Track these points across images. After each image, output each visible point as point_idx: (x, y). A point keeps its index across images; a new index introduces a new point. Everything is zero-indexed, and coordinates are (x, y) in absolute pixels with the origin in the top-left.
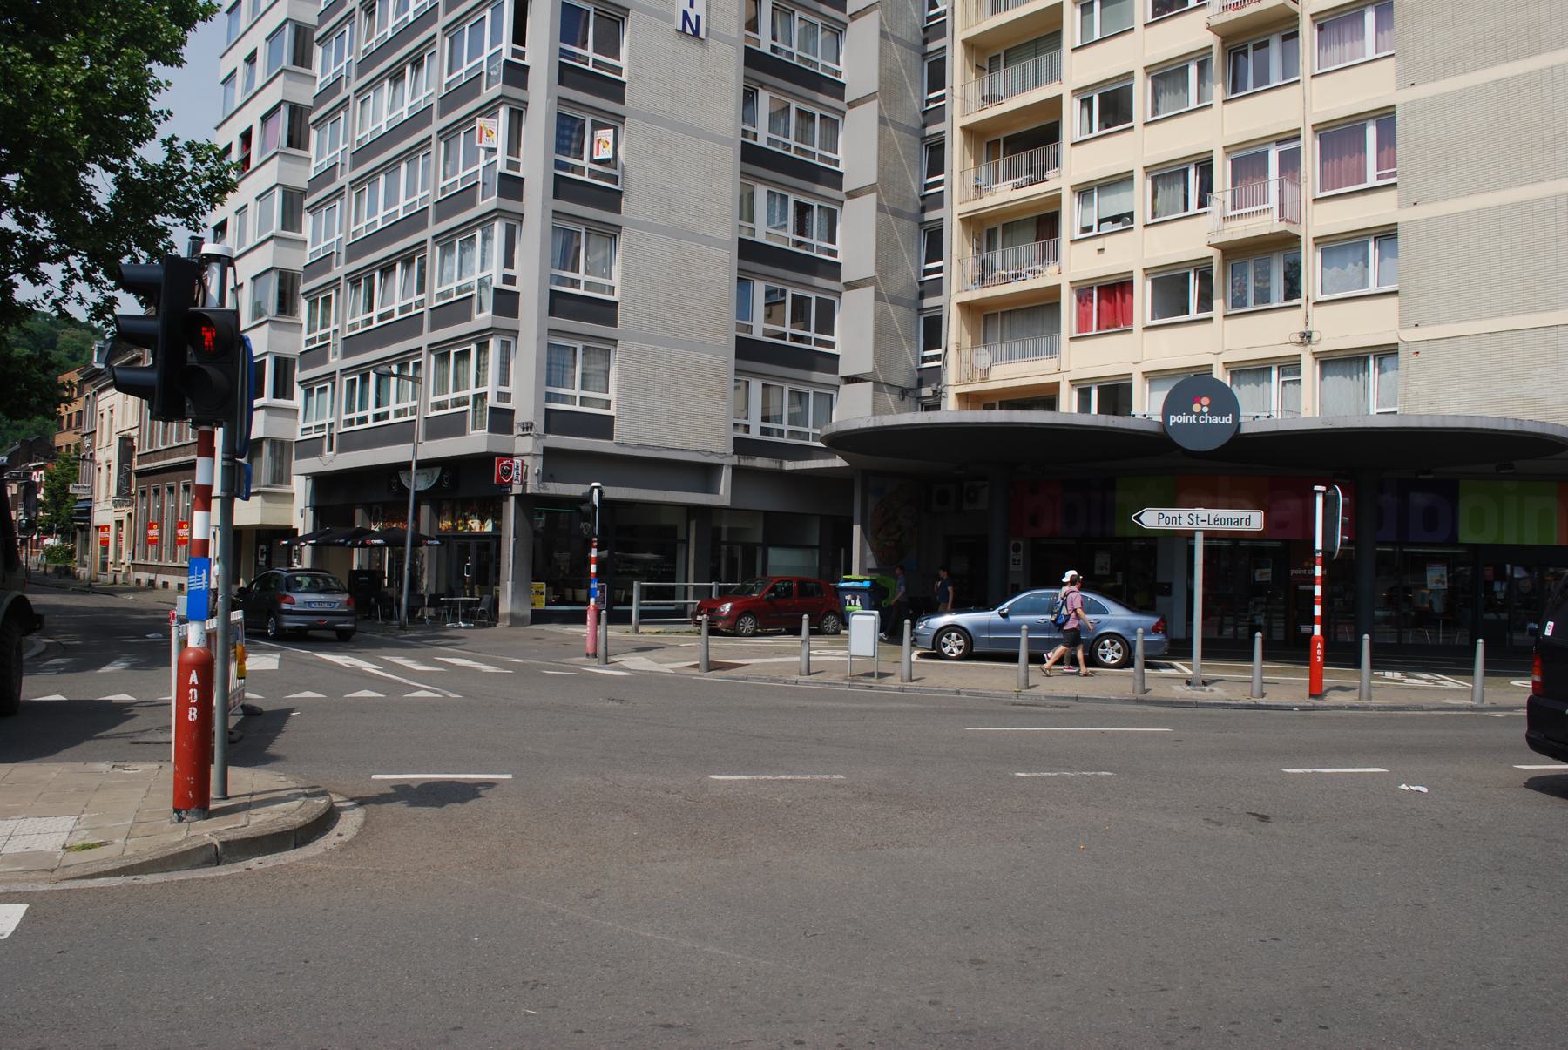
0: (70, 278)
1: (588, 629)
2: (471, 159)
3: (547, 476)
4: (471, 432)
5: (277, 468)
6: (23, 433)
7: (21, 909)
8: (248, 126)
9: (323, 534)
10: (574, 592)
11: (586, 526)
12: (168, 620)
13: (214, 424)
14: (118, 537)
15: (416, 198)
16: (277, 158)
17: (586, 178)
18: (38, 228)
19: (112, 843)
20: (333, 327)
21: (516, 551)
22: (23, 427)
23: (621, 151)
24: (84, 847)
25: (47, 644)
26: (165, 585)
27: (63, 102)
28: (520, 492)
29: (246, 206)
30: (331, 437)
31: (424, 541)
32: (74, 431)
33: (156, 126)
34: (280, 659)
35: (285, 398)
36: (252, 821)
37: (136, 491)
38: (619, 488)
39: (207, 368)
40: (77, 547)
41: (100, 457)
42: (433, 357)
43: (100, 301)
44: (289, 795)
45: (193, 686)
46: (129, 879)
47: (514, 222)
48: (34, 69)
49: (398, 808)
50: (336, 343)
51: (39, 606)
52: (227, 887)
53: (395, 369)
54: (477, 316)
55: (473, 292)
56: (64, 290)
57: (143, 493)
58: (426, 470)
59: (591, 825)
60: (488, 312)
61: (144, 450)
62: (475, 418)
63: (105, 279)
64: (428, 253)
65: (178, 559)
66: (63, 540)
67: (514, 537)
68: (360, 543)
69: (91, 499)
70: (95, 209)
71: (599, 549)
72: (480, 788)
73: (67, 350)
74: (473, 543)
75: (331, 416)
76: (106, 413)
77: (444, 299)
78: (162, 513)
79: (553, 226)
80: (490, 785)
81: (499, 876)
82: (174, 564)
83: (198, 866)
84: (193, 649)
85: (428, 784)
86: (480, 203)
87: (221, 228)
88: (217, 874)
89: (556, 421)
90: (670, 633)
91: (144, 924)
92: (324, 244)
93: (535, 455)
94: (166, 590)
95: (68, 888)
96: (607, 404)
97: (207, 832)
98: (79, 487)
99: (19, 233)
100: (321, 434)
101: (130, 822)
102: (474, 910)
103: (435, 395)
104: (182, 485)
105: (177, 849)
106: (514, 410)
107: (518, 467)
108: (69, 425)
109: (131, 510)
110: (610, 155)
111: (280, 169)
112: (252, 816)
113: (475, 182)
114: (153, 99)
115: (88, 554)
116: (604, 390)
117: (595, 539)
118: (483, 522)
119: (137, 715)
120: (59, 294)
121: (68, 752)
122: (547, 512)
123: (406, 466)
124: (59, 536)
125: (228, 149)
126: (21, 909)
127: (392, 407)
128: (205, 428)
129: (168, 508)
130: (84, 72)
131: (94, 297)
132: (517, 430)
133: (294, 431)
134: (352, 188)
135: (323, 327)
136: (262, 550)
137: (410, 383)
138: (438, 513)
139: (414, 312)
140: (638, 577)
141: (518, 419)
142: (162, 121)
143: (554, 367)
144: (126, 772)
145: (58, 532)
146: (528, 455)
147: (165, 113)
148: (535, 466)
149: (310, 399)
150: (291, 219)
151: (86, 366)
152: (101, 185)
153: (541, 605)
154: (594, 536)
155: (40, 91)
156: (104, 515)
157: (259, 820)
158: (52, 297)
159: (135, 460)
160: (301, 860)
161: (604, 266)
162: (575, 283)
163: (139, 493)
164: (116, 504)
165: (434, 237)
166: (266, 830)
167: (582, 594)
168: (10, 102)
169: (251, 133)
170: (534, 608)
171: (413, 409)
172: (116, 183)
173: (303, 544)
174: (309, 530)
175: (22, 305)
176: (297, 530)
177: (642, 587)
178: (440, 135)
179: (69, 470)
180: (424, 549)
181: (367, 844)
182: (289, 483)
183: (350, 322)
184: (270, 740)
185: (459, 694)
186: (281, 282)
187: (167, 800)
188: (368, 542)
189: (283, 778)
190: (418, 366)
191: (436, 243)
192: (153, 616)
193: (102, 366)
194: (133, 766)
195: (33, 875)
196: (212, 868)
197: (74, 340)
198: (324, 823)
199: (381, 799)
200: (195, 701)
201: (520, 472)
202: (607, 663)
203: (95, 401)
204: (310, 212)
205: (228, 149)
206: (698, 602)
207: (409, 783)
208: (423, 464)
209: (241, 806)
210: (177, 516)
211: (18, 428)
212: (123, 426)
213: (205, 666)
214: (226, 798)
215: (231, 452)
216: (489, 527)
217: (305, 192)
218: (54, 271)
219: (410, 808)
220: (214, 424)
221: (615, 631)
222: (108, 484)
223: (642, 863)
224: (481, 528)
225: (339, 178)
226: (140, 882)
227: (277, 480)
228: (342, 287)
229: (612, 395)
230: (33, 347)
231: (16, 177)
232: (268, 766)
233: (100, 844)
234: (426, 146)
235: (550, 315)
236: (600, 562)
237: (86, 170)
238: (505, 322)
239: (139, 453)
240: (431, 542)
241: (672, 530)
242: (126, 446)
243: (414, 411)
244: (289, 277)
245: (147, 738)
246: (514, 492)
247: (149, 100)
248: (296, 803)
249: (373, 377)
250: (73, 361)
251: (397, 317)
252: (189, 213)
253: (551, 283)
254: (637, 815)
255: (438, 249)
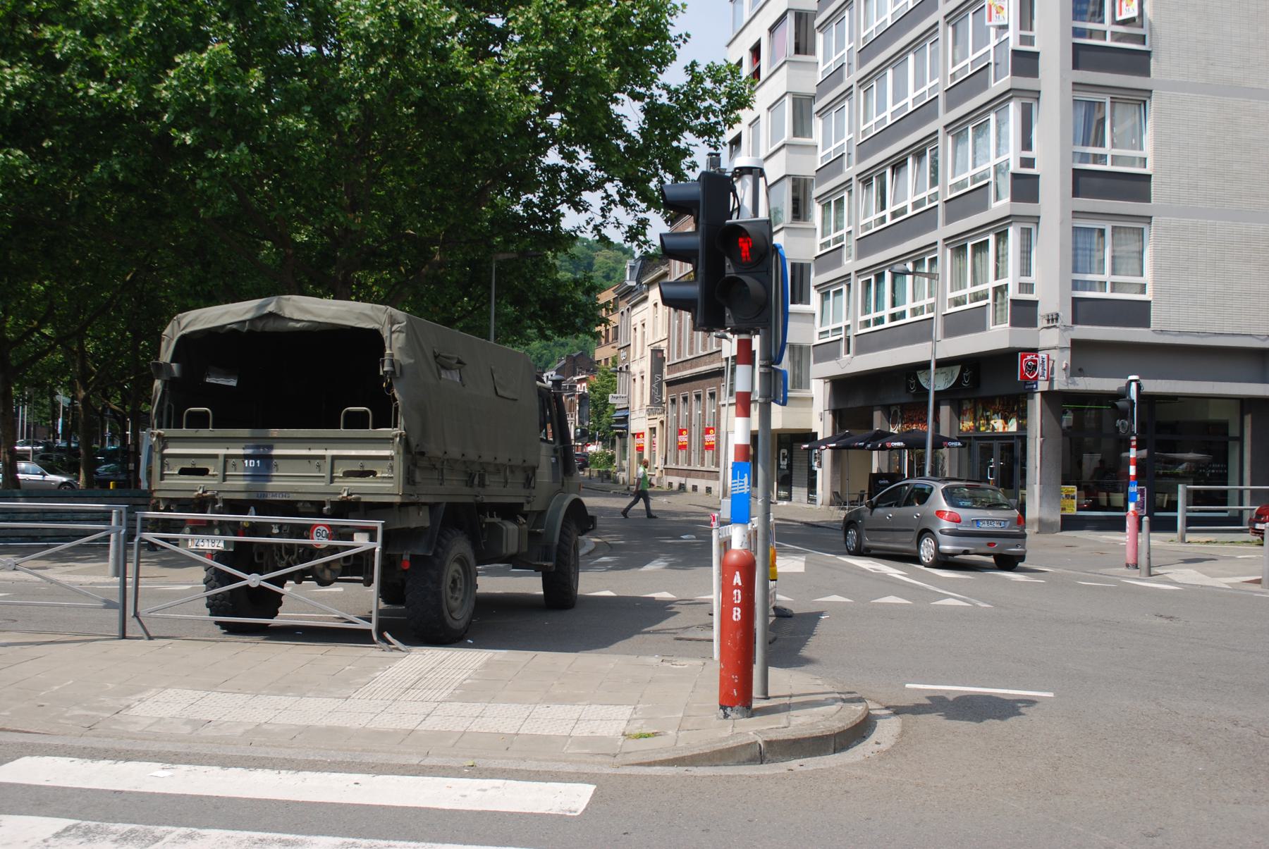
0: (609, 204)
1: (1128, 537)
2: (982, 39)
3: (1076, 370)
4: (991, 328)
5: (796, 372)
6: (568, 349)
7: (590, 789)
8: (755, 40)
9: (842, 438)
10: (1108, 496)
11: (1122, 424)
12: (709, 523)
13: (752, 332)
14: (652, 444)
15: (925, 88)
16: (785, 67)
17: (1108, 42)
18: (578, 159)
19: (665, 734)
20: (846, 229)
21: (1044, 452)
22: (567, 344)
23: (1146, 7)
24: (641, 736)
25: (596, 543)
26: (695, 488)
27: (595, 40)
28: (1046, 389)
29: (759, 117)
30: (848, 340)
31: (945, 443)
32: (611, 346)
33: (676, 50)
34: (806, 562)
35: (802, 303)
36: (793, 723)
37: (667, 399)
38: (1159, 381)
39: (745, 278)
40: (617, 453)
41: (634, 368)
42: (949, 251)
43: (634, 223)
44: (826, 699)
45: (737, 587)
46: (681, 770)
47: (1030, 101)
48: (569, 14)
49: (935, 720)
50: (850, 244)
51: (592, 508)
52: (771, 786)
53: (910, 266)
54: (994, 205)
55: (989, 180)
56: (604, 216)
57: (673, 401)
58: (944, 369)
59: (1147, 755)
60: (1006, 200)
61: (673, 360)
62: (995, 311)
63: (638, 202)
64: (940, 144)
65: (928, 469)
66: (604, 447)
67: (1041, 437)
68: (880, 445)
69: (628, 408)
70: (628, 137)
71: (1138, 448)
72: (1019, 705)
73: (602, 271)
74: (996, 445)
75: (847, 319)
76: (639, 327)
77: (958, 190)
78: (691, 419)
79: (1074, 100)
80: (1030, 702)
81: (1047, 802)
82: (702, 469)
83: (743, 763)
84: (737, 551)
85: (965, 696)
86: (993, 85)
87: (736, 141)
88: (762, 773)
89: (1083, 311)
90: (1223, 543)
91: (698, 815)
92: (834, 146)
93: (1061, 348)
94: (695, 494)
95: (628, 773)
96: (1142, 289)
97: (753, 730)
98: (617, 398)
99: (563, 166)
100: (837, 338)
101: (681, 715)
102: (1022, 836)
103: (952, 291)
104: (707, 392)
105: (724, 745)
106: (1037, 302)
107: (1043, 362)
108: (607, 341)
109: (662, 417)
110: (1135, 14)
111: (789, 77)
112: (793, 718)
113: (986, 63)
114: (672, 25)
115: (625, 459)
116: (1139, 273)
117: (1134, 438)
118: (1006, 422)
119: (677, 613)
120: (599, 220)
121: (621, 644)
122: (1073, 410)
123: (925, 366)
124: (600, 443)
125: (740, 63)
126: (590, 789)
127: (908, 306)
128: (744, 337)
129: (695, 415)
130: (611, 10)
131: (628, 220)
132: (1042, 322)
133: (812, 335)
134: (860, 86)
135: (836, 230)
136: (784, 454)
137: (926, 279)
138: (958, 413)
139: (928, 206)
140: (1183, 478)
141: (1042, 310)
142: (682, 44)
143: (1080, 252)
144: (675, 666)
145: (600, 439)
146: (1055, 348)
147: (684, 36)
148: (1063, 360)
149: (825, 302)
150: (801, 124)
151: (621, 283)
152: (630, 114)
153: (1072, 511)
154: (1133, 434)
155: (575, 34)
156: (639, 423)
157: (799, 722)
158: (592, 224)
159: (665, 370)
160: (841, 766)
161: (1134, 136)
162: (1100, 158)
163: (670, 401)
164: (649, 412)
165: (946, 127)
166: (807, 733)
167: (1118, 498)
168: (551, 47)
169: (760, 45)
170: (1064, 513)
171: (929, 306)
172: (644, 110)
173: (823, 447)
174: (829, 434)
175: (568, 232)
176: (816, 434)
177: (1188, 491)
178: (947, 20)
179: (608, 382)
180: (945, 451)
181: (906, 755)
182: (808, 387)
183: (863, 222)
184: (803, 643)
185: (989, 604)
186: (795, 189)
187: (711, 692)
188: (888, 444)
189: (819, 682)
190: (933, 261)
191: (948, 133)
192: (685, 518)
193: (634, 283)
194: (680, 661)
195: (599, 758)
196: (757, 766)
197: (608, 261)
198: (860, 730)
199: (916, 709)
200: (739, 602)
201: (1046, 368)
202: (1150, 575)
203: (629, 317)
204: (820, 116)
205: (740, 63)
206: (1257, 508)
207: (944, 695)
208: (942, 363)
209: (782, 707)
210: (704, 422)
211: (563, 345)
212: (654, 338)
213: (747, 569)
214: (767, 698)
215: (771, 359)
216: (1013, 427)
217: (814, 97)
218: (593, 198)
219: (948, 721)
220: (752, 332)
221: (1159, 540)
222: (642, 394)
223: (1210, 802)
224: (1004, 428)
225: (846, 79)
226: (692, 773)
227: (796, 384)
228: (854, 188)
229: (1148, 277)
230: (573, 270)
231: (558, 115)
232: (802, 668)
233: (655, 734)
234: (934, 32)
235: (1073, 196)
236: (1139, 463)
237: (616, 101)
238: (1025, 208)
239: (669, 363)
240: (953, 443)
241: (1222, 427)
242: (658, 357)
243: (931, 308)
244: (802, 182)
245: (689, 635)
246: (1040, 389)
247: (669, 27)
248: (834, 708)
249: (888, 275)
250: (608, 281)
251: (910, 213)
252: (708, 131)
253: (1073, 161)
254: (1201, 749)
255: (950, 138)
